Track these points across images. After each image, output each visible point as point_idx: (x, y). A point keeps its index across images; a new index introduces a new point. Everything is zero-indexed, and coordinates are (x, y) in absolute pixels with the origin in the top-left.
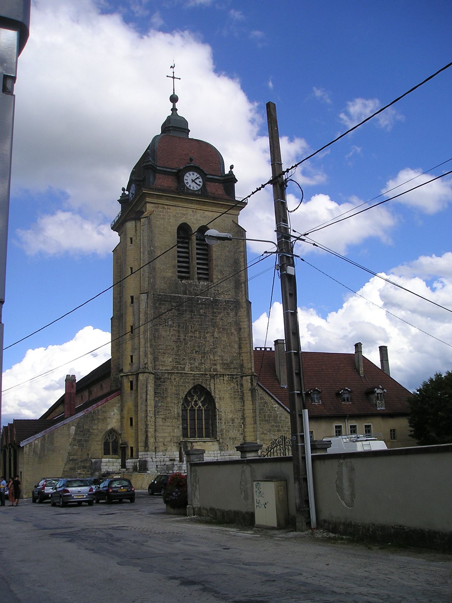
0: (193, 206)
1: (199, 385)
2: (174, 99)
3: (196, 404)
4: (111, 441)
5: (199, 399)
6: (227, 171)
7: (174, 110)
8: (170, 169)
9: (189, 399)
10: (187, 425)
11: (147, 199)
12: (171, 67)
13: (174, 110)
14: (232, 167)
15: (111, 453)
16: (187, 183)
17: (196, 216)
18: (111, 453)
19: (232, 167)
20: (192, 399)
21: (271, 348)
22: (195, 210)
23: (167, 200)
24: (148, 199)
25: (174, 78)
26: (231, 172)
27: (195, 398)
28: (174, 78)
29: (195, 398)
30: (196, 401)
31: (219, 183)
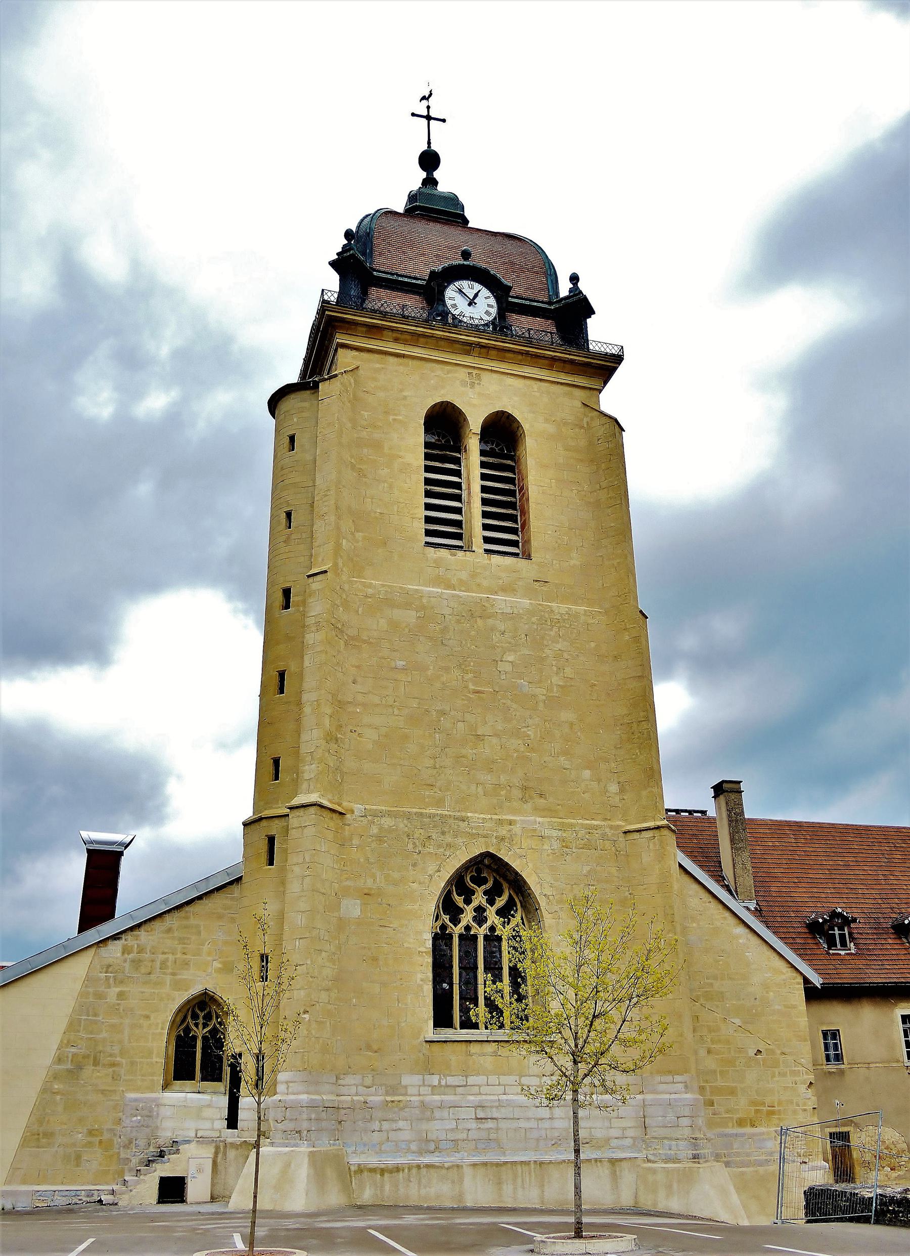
0: (468, 360)
1: (488, 855)
2: (429, 160)
3: (480, 918)
4: (200, 1032)
5: (491, 902)
6: (564, 289)
7: (429, 182)
8: (410, 277)
9: (459, 900)
10: (451, 985)
11: (337, 335)
12: (424, 98)
13: (429, 182)
14: (574, 279)
15: (198, 1074)
16: (454, 306)
17: (480, 392)
18: (198, 1074)
19: (574, 279)
20: (468, 901)
21: (704, 812)
22: (475, 372)
23: (396, 340)
24: (340, 338)
25: (429, 118)
26: (575, 291)
27: (479, 898)
28: (429, 118)
29: (479, 898)
30: (480, 910)
31: (547, 318)
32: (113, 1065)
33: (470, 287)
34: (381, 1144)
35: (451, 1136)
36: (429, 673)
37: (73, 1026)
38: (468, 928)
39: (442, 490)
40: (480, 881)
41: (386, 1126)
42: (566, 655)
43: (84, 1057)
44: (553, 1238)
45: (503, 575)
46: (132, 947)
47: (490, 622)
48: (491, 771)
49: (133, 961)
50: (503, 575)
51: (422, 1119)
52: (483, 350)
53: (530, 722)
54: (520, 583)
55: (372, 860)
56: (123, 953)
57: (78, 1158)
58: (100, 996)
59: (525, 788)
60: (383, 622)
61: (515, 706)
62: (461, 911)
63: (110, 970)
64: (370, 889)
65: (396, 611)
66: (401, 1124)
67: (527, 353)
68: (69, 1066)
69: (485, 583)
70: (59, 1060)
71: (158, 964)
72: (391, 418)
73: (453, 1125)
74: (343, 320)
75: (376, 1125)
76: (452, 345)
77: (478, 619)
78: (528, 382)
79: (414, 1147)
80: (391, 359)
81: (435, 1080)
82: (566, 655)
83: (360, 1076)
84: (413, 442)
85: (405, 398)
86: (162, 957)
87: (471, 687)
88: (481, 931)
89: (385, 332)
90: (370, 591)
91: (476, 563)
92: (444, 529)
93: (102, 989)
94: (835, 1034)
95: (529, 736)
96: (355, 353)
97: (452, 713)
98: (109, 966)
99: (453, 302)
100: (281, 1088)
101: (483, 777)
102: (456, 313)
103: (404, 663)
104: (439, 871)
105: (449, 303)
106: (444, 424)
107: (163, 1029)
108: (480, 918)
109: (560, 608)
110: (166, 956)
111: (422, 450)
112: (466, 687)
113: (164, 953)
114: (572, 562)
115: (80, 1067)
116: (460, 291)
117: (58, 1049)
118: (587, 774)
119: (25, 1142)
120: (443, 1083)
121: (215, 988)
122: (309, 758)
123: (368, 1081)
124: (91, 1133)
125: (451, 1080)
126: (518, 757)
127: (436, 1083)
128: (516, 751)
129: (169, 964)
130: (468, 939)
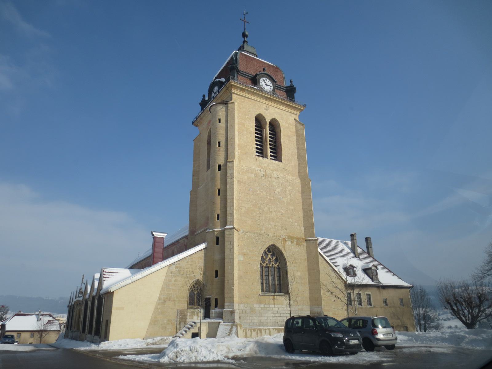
8: (249, 74)
9: (265, 257)
22: (268, 106)
32: (174, 301)
33: (268, 82)
34: (250, 323)
35: (266, 321)
36: (258, 192)
37: (163, 289)
38: (267, 264)
39: (260, 139)
40: (270, 252)
41: (251, 318)
42: (291, 191)
43: (166, 298)
44: (414, 347)
45: (275, 166)
46: (178, 266)
47: (273, 179)
48: (273, 222)
49: (178, 270)
50: (275, 166)
51: (259, 316)
52: (271, 100)
53: (283, 208)
54: (280, 169)
55: (245, 245)
56: (176, 268)
57: (166, 328)
58: (170, 281)
59: (282, 227)
60: (246, 177)
61: (279, 204)
62: (265, 260)
63: (172, 273)
64: (245, 253)
65: (249, 174)
66: (255, 318)
67: (282, 102)
68: (162, 301)
69: (271, 168)
70: (159, 299)
71: (185, 272)
72: (247, 117)
73: (266, 318)
74: (235, 86)
75: (248, 318)
76: (262, 97)
77: (270, 178)
78: (281, 111)
79: (258, 324)
80: (246, 99)
81: (262, 306)
82: (291, 191)
83: (244, 304)
84: (252, 125)
85: (250, 111)
86: (186, 270)
87: (268, 197)
88: (271, 265)
89: (245, 91)
90: (243, 168)
91: (268, 162)
92: (261, 152)
93: (170, 279)
94: (369, 295)
95: (282, 212)
96: (237, 96)
97: (264, 204)
98: (172, 272)
99: (262, 84)
100: (225, 307)
101: (272, 223)
102: (263, 87)
103: (251, 189)
104: (262, 249)
105: (261, 84)
106: (259, 121)
107: (187, 290)
108: (270, 262)
109: (289, 177)
110: (187, 269)
111: (254, 128)
112: (267, 197)
113: (186, 269)
114: (292, 164)
115: (165, 301)
116: (264, 81)
117: (159, 296)
118: (296, 224)
119: (150, 324)
120: (264, 307)
121: (191, 278)
122: (230, 215)
123: (246, 306)
124: (169, 320)
125: (266, 306)
126: (280, 218)
127: (262, 306)
128: (280, 216)
129: (188, 272)
130: (267, 267)
